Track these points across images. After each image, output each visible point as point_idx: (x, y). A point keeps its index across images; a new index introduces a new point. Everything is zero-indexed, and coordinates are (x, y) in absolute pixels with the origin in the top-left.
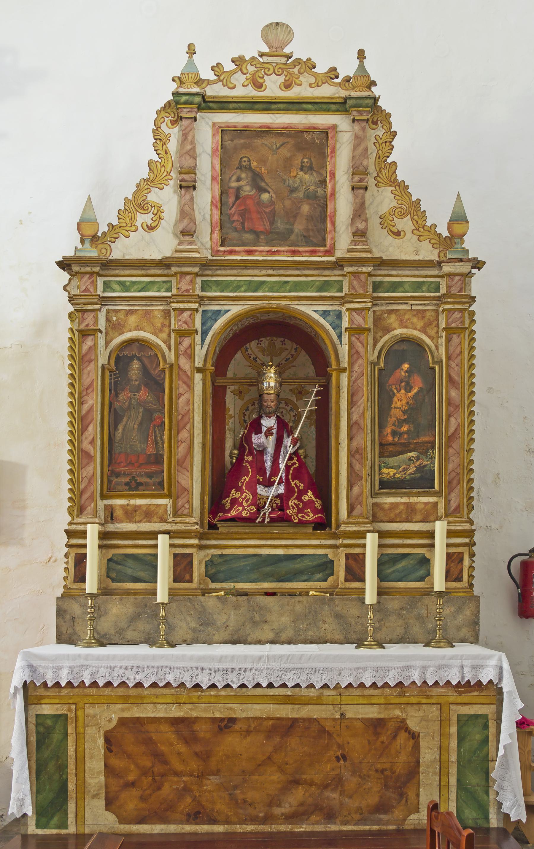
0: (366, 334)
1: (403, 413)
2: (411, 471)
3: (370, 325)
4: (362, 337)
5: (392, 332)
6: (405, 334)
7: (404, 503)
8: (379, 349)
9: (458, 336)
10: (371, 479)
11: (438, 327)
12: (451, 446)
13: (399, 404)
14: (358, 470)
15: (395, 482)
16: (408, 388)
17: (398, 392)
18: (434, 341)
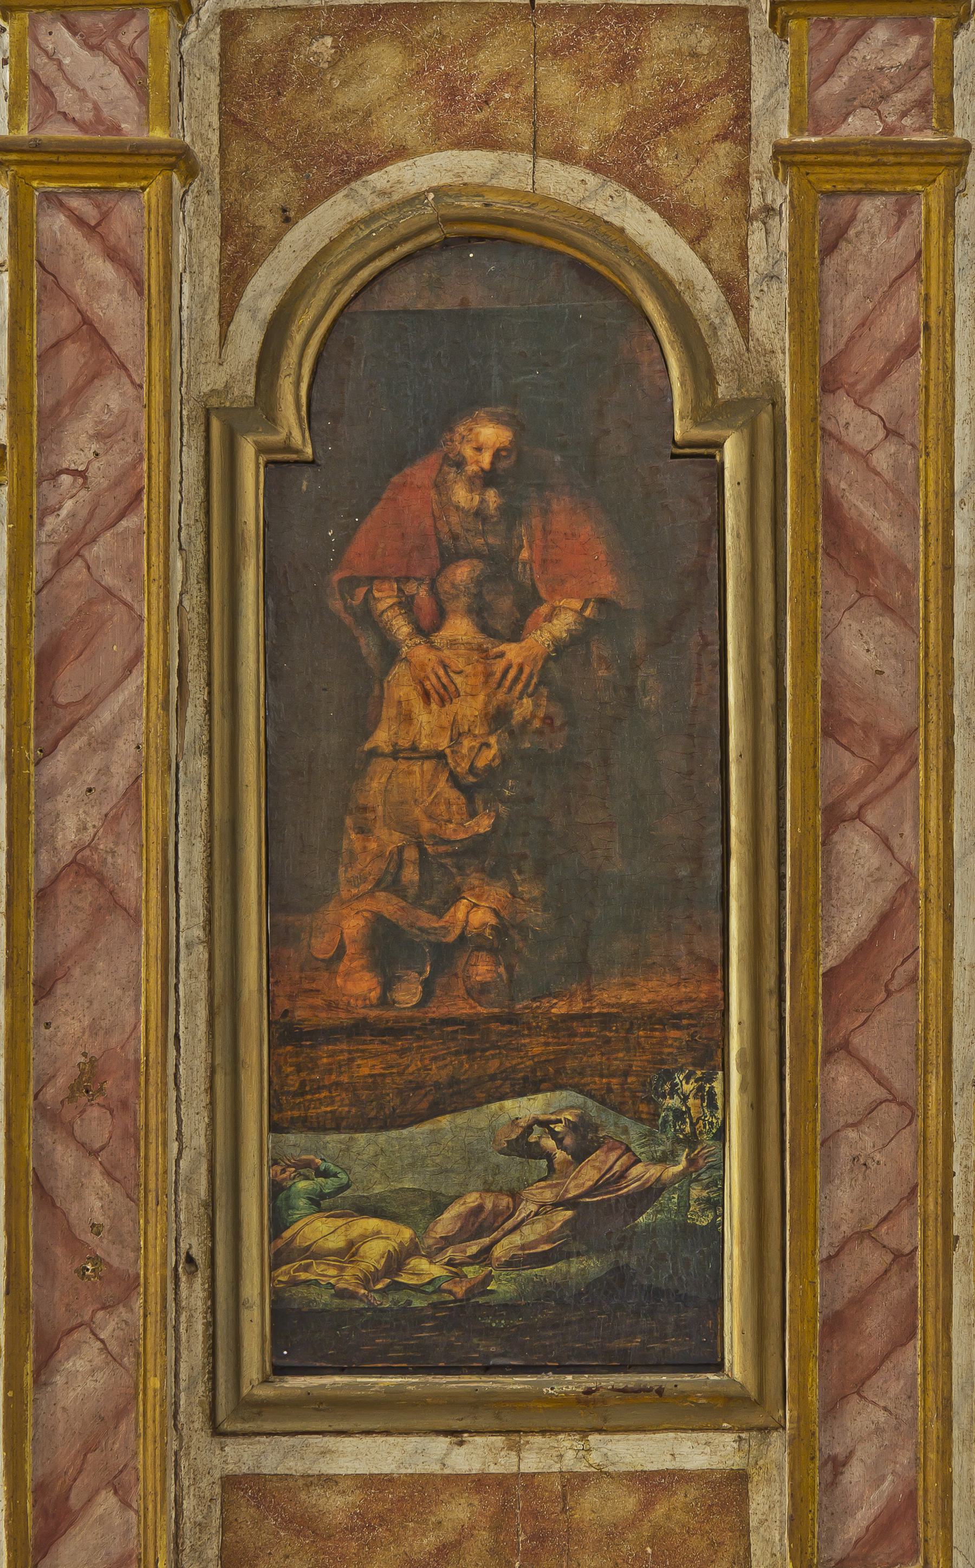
0: (152, 194)
1: (468, 791)
2: (530, 1233)
3: (201, 130)
4: (125, 213)
5: (377, 179)
6: (477, 190)
7: (479, 1482)
8: (268, 306)
9: (902, 213)
10: (212, 1295)
11: (746, 141)
12: (845, 1046)
13: (428, 725)
14: (96, 1229)
15: (407, 1318)
16: (505, 604)
17: (425, 631)
18: (714, 244)
